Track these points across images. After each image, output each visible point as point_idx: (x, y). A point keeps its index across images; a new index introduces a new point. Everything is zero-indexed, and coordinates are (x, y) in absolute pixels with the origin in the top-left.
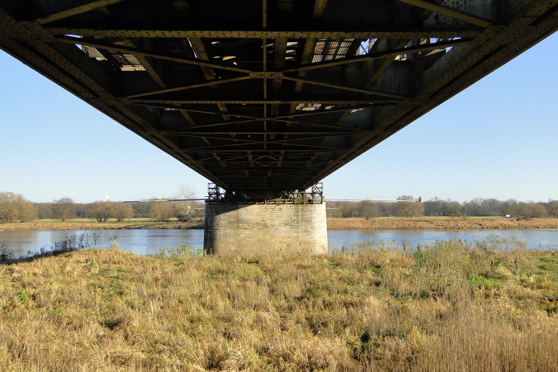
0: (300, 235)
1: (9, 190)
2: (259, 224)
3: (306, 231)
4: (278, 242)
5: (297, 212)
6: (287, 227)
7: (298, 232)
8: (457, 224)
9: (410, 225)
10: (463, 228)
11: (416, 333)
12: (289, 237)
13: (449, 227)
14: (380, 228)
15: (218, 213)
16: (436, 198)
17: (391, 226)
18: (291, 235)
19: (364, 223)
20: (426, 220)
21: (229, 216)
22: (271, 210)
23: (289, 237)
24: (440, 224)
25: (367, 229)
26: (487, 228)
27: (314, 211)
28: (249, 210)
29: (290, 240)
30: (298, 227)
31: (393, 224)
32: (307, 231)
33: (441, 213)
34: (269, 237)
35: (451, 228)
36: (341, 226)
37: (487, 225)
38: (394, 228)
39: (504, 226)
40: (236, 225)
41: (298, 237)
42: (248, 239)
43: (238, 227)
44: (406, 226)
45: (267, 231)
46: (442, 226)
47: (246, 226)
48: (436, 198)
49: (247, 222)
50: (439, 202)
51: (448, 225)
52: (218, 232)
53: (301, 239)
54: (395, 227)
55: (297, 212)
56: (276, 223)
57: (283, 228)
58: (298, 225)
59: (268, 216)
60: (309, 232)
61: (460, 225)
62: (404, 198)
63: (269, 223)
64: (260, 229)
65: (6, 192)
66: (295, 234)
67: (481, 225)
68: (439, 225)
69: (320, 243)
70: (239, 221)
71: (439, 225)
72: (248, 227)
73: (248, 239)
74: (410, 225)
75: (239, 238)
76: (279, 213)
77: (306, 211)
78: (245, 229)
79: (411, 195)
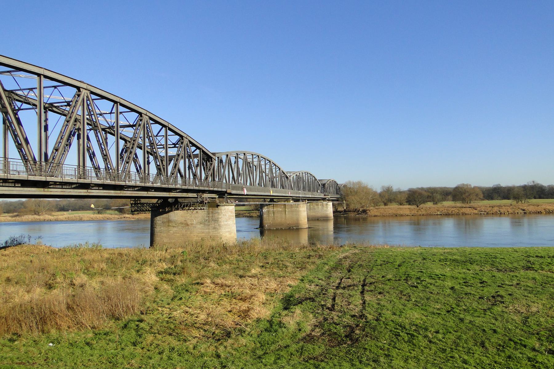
0: (210, 231)
2: (183, 223)
3: (214, 228)
4: (195, 236)
5: (209, 214)
6: (202, 225)
7: (209, 229)
8: (500, 209)
10: (504, 214)
12: (203, 233)
13: (491, 212)
14: (425, 214)
15: (156, 216)
16: (533, 182)
18: (204, 231)
20: (471, 206)
21: (163, 218)
22: (191, 213)
23: (203, 233)
24: (483, 210)
25: (412, 215)
26: (530, 213)
27: (220, 213)
28: (176, 213)
29: (204, 234)
30: (209, 225)
31: (438, 211)
32: (215, 228)
33: (537, 196)
34: (189, 233)
35: (493, 214)
36: (390, 214)
37: (530, 210)
38: (438, 215)
39: (548, 211)
40: (167, 224)
41: (209, 232)
42: (175, 234)
43: (169, 226)
45: (188, 228)
47: (174, 224)
48: (533, 182)
49: (175, 222)
50: (535, 185)
52: (156, 229)
53: (211, 234)
54: (439, 214)
55: (209, 214)
56: (193, 222)
57: (199, 226)
58: (209, 223)
59: (189, 217)
60: (216, 229)
61: (502, 211)
63: (189, 222)
64: (183, 227)
66: (207, 231)
67: (524, 210)
68: (482, 211)
69: (226, 237)
70: (169, 221)
71: (482, 211)
72: (175, 226)
73: (175, 234)
75: (169, 233)
76: (196, 215)
77: (215, 214)
78: (173, 227)
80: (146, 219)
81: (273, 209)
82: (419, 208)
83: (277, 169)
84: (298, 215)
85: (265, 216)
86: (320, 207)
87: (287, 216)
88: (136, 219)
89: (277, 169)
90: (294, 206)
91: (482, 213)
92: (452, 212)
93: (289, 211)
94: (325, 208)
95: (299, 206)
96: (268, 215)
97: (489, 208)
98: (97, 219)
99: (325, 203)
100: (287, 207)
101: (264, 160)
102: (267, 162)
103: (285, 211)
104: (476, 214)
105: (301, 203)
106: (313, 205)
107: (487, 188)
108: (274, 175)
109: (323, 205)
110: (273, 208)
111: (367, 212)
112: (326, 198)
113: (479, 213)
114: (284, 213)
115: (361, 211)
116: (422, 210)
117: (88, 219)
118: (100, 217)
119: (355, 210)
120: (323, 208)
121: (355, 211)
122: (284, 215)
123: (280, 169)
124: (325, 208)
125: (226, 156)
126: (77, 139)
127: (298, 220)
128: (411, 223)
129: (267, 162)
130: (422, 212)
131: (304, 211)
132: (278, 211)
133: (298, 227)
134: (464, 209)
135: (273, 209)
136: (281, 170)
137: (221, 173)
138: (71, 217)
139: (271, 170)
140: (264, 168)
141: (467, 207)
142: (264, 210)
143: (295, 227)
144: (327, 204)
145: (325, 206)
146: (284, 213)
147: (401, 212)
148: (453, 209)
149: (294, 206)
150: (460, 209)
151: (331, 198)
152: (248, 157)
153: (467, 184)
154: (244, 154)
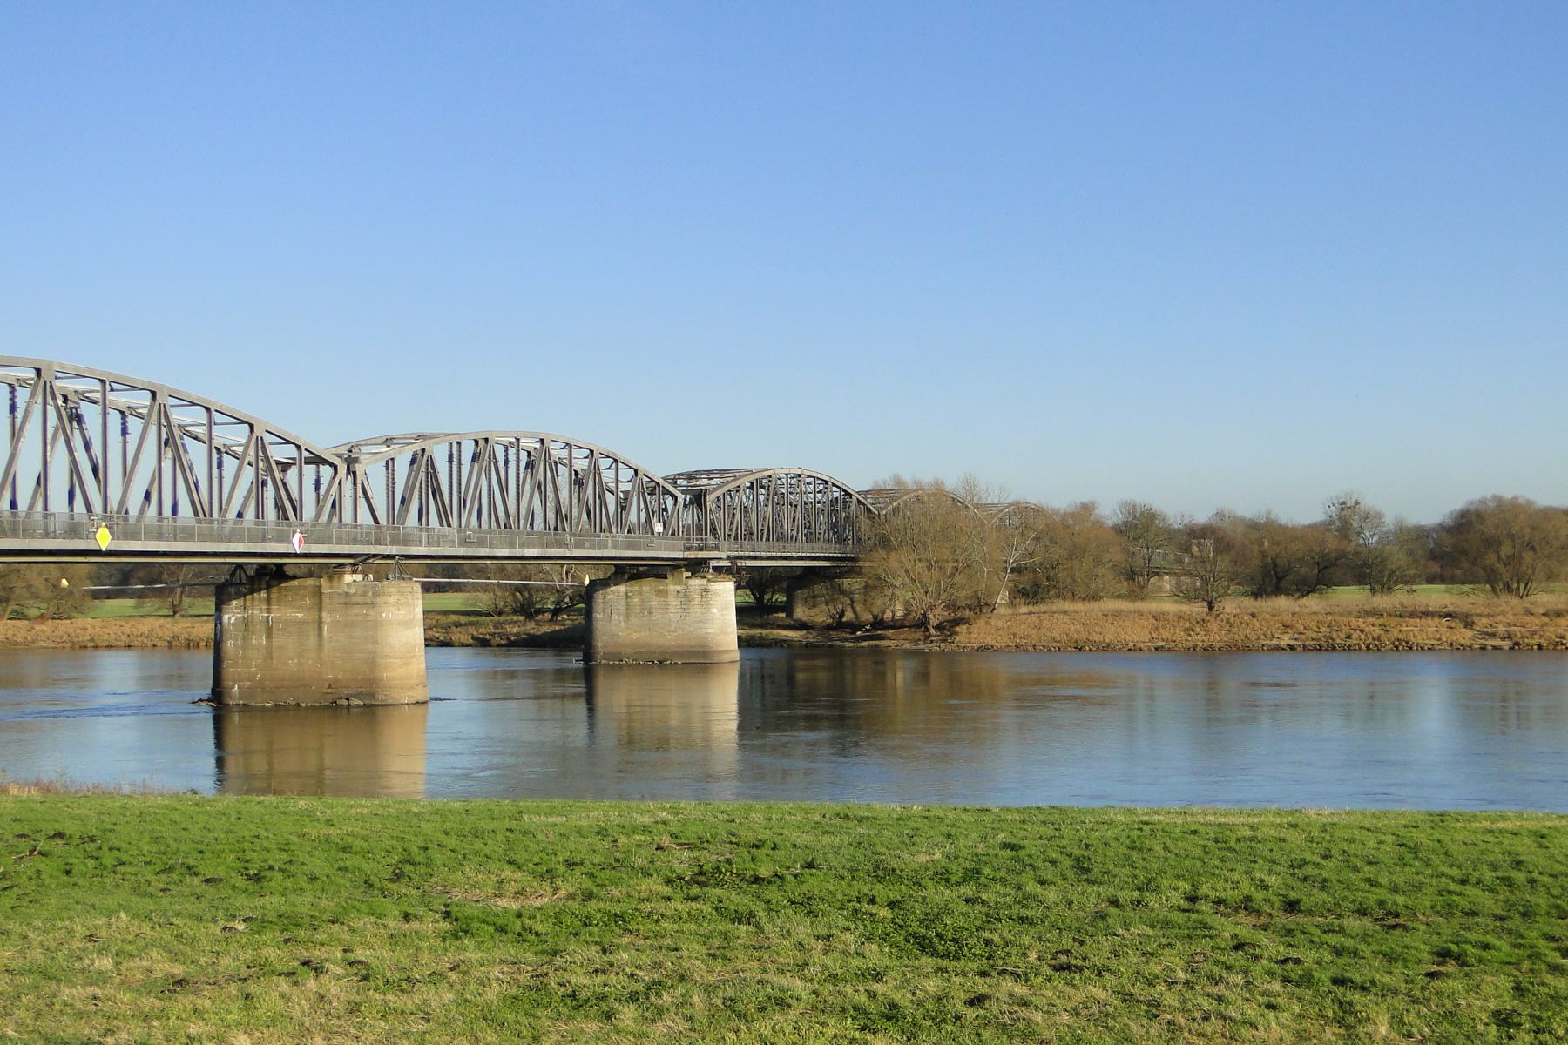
13: (1536, 640)
24: (1501, 629)
25: (1157, 649)
35: (1540, 647)
36: (1054, 639)
38: (1278, 648)
44: (1339, 639)
71: (1493, 635)
74: (1355, 635)
81: (269, 611)
84: (376, 642)
85: (229, 645)
86: (674, 603)
87: (326, 644)
95: (379, 600)
96: (244, 639)
99: (696, 583)
100: (326, 600)
103: (320, 623)
109: (686, 596)
110: (264, 607)
112: (705, 561)
114: (311, 631)
122: (312, 641)
124: (696, 610)
126: (10, 413)
127: (372, 663)
128: (151, 678)
130: (1207, 632)
132: (286, 623)
133: (372, 696)
135: (269, 611)
137: (460, 485)
143: (357, 696)
144: (705, 591)
145: (697, 600)
149: (359, 599)
150: (1393, 621)
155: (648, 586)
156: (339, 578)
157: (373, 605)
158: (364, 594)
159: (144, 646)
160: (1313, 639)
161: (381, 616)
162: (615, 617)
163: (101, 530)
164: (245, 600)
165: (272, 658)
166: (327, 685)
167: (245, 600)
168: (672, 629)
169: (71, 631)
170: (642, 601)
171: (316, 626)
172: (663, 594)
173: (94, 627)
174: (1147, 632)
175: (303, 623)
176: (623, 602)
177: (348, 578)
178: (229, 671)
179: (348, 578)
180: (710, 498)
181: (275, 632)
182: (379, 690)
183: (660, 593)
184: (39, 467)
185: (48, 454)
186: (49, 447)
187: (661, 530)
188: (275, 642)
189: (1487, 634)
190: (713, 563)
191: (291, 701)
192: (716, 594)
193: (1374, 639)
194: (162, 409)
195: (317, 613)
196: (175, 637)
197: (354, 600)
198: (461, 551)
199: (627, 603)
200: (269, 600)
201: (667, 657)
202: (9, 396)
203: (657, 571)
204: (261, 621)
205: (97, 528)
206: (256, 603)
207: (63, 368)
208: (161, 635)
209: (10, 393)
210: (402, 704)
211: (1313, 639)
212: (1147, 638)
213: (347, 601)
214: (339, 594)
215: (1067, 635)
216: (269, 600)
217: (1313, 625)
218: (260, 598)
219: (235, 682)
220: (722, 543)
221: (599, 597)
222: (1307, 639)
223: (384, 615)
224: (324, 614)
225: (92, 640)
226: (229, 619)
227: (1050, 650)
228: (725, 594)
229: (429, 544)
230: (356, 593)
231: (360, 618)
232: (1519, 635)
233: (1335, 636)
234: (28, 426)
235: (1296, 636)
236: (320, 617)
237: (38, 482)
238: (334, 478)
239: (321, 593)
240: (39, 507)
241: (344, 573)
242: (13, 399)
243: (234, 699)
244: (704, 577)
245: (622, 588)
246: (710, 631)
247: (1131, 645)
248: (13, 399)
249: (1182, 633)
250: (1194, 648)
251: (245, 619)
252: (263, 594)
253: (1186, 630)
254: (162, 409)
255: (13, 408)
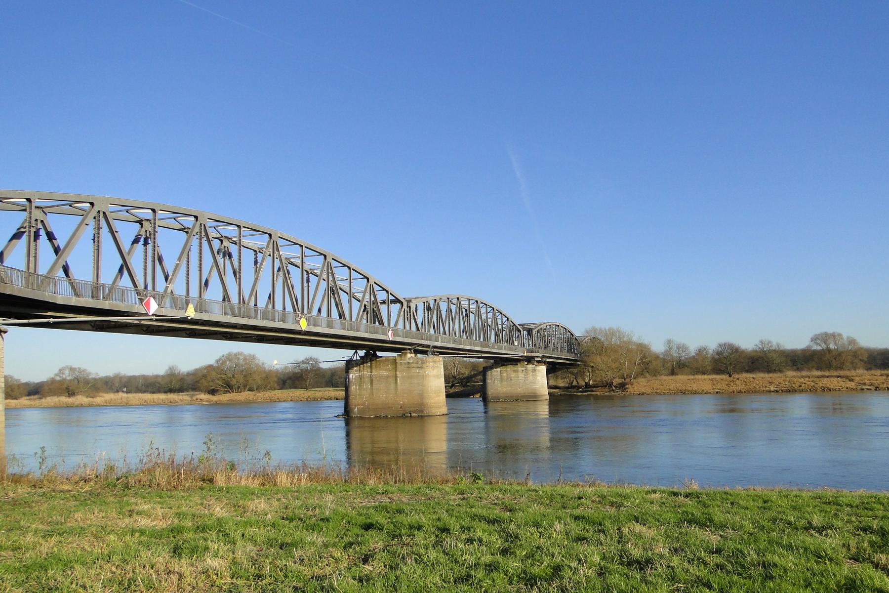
1: (553, 321)
9: (803, 385)
11: (873, 504)
14: (743, 390)
17: (766, 387)
19: (715, 383)
24: (867, 382)
25: (717, 393)
31: (771, 383)
38: (770, 391)
44: (796, 386)
46: (870, 386)
51: (883, 383)
62: (825, 337)
65: (235, 352)
68: (865, 384)
71: (865, 384)
74: (803, 385)
79: (838, 330)
80: (230, 402)
81: (371, 372)
82: (732, 378)
83: (504, 320)
84: (423, 386)
86: (521, 375)
87: (399, 387)
88: (212, 403)
89: (504, 320)
90: (415, 365)
91: (864, 387)
92: (800, 386)
93: (403, 377)
94: (531, 378)
95: (424, 365)
96: (360, 386)
97: (880, 377)
98: (154, 402)
99: (530, 367)
100: (399, 366)
101: (485, 306)
102: (489, 309)
103: (396, 377)
104: (852, 389)
105: (430, 358)
106: (507, 371)
107: (881, 350)
108: (500, 327)
109: (526, 371)
110: (369, 370)
111: (627, 386)
112: (533, 358)
113: (859, 387)
114: (392, 380)
115: (614, 384)
116: (738, 382)
117: (137, 403)
118: (159, 399)
119: (605, 384)
120: (526, 377)
121: (606, 386)
122: (392, 386)
123: (508, 319)
124: (531, 378)
125: (433, 301)
127: (421, 396)
129: (489, 309)
131: (438, 377)
132: (380, 377)
133: (422, 411)
134: (825, 379)
135: (371, 372)
136: (509, 321)
138: (115, 400)
139: (495, 319)
140: (485, 318)
141: (832, 376)
142: (351, 376)
143: (414, 412)
144: (534, 370)
146: (394, 382)
147: (695, 387)
148: (802, 379)
149: (415, 365)
150: (818, 380)
151: (543, 357)
152: (462, 303)
153: (834, 333)
154: (458, 298)
155: (509, 368)
156: (405, 355)
157: (421, 367)
158: (417, 363)
159: (297, 401)
160: (784, 387)
161: (425, 373)
162: (496, 381)
163: (302, 319)
164: (360, 367)
165: (373, 395)
166: (400, 407)
167: (360, 367)
168: (521, 386)
169: (270, 395)
170: (507, 375)
171: (394, 379)
172: (517, 371)
173: (278, 394)
174: (710, 386)
175: (388, 377)
176: (499, 375)
177: (409, 355)
178: (353, 400)
179: (409, 355)
180: (534, 331)
181: (374, 382)
182: (425, 409)
183: (515, 371)
184: (270, 289)
185: (275, 279)
186: (275, 276)
187: (517, 344)
188: (375, 386)
189: (860, 383)
190: (536, 359)
191: (383, 415)
192: (539, 371)
193: (812, 387)
194: (329, 264)
195: (394, 373)
196: (309, 397)
197: (413, 365)
198: (453, 346)
199: (501, 376)
200: (371, 367)
201: (519, 398)
202: (254, 257)
203: (514, 361)
204: (367, 377)
205: (300, 318)
206: (365, 368)
207: (282, 236)
208: (303, 396)
209: (255, 255)
210: (436, 415)
211: (784, 387)
212: (711, 388)
213: (409, 366)
214: (405, 363)
215: (676, 388)
216: (371, 367)
217: (782, 381)
218: (367, 366)
219: (355, 406)
220: (541, 350)
221: (489, 373)
222: (782, 387)
223: (427, 372)
224: (398, 373)
225: (278, 399)
226: (353, 376)
227: (671, 394)
228: (543, 369)
229: (442, 342)
230: (413, 362)
231: (415, 374)
232: (876, 384)
233: (794, 386)
234: (264, 263)
235: (776, 386)
236: (396, 375)
237: (269, 297)
238: (402, 308)
239: (396, 363)
240: (270, 306)
241: (407, 353)
242: (256, 258)
243: (355, 414)
244: (534, 364)
245: (499, 369)
246: (538, 387)
247: (705, 391)
248: (256, 258)
249: (726, 386)
250: (734, 392)
251: (360, 376)
252: (369, 364)
253: (727, 385)
254: (329, 264)
255: (256, 263)
